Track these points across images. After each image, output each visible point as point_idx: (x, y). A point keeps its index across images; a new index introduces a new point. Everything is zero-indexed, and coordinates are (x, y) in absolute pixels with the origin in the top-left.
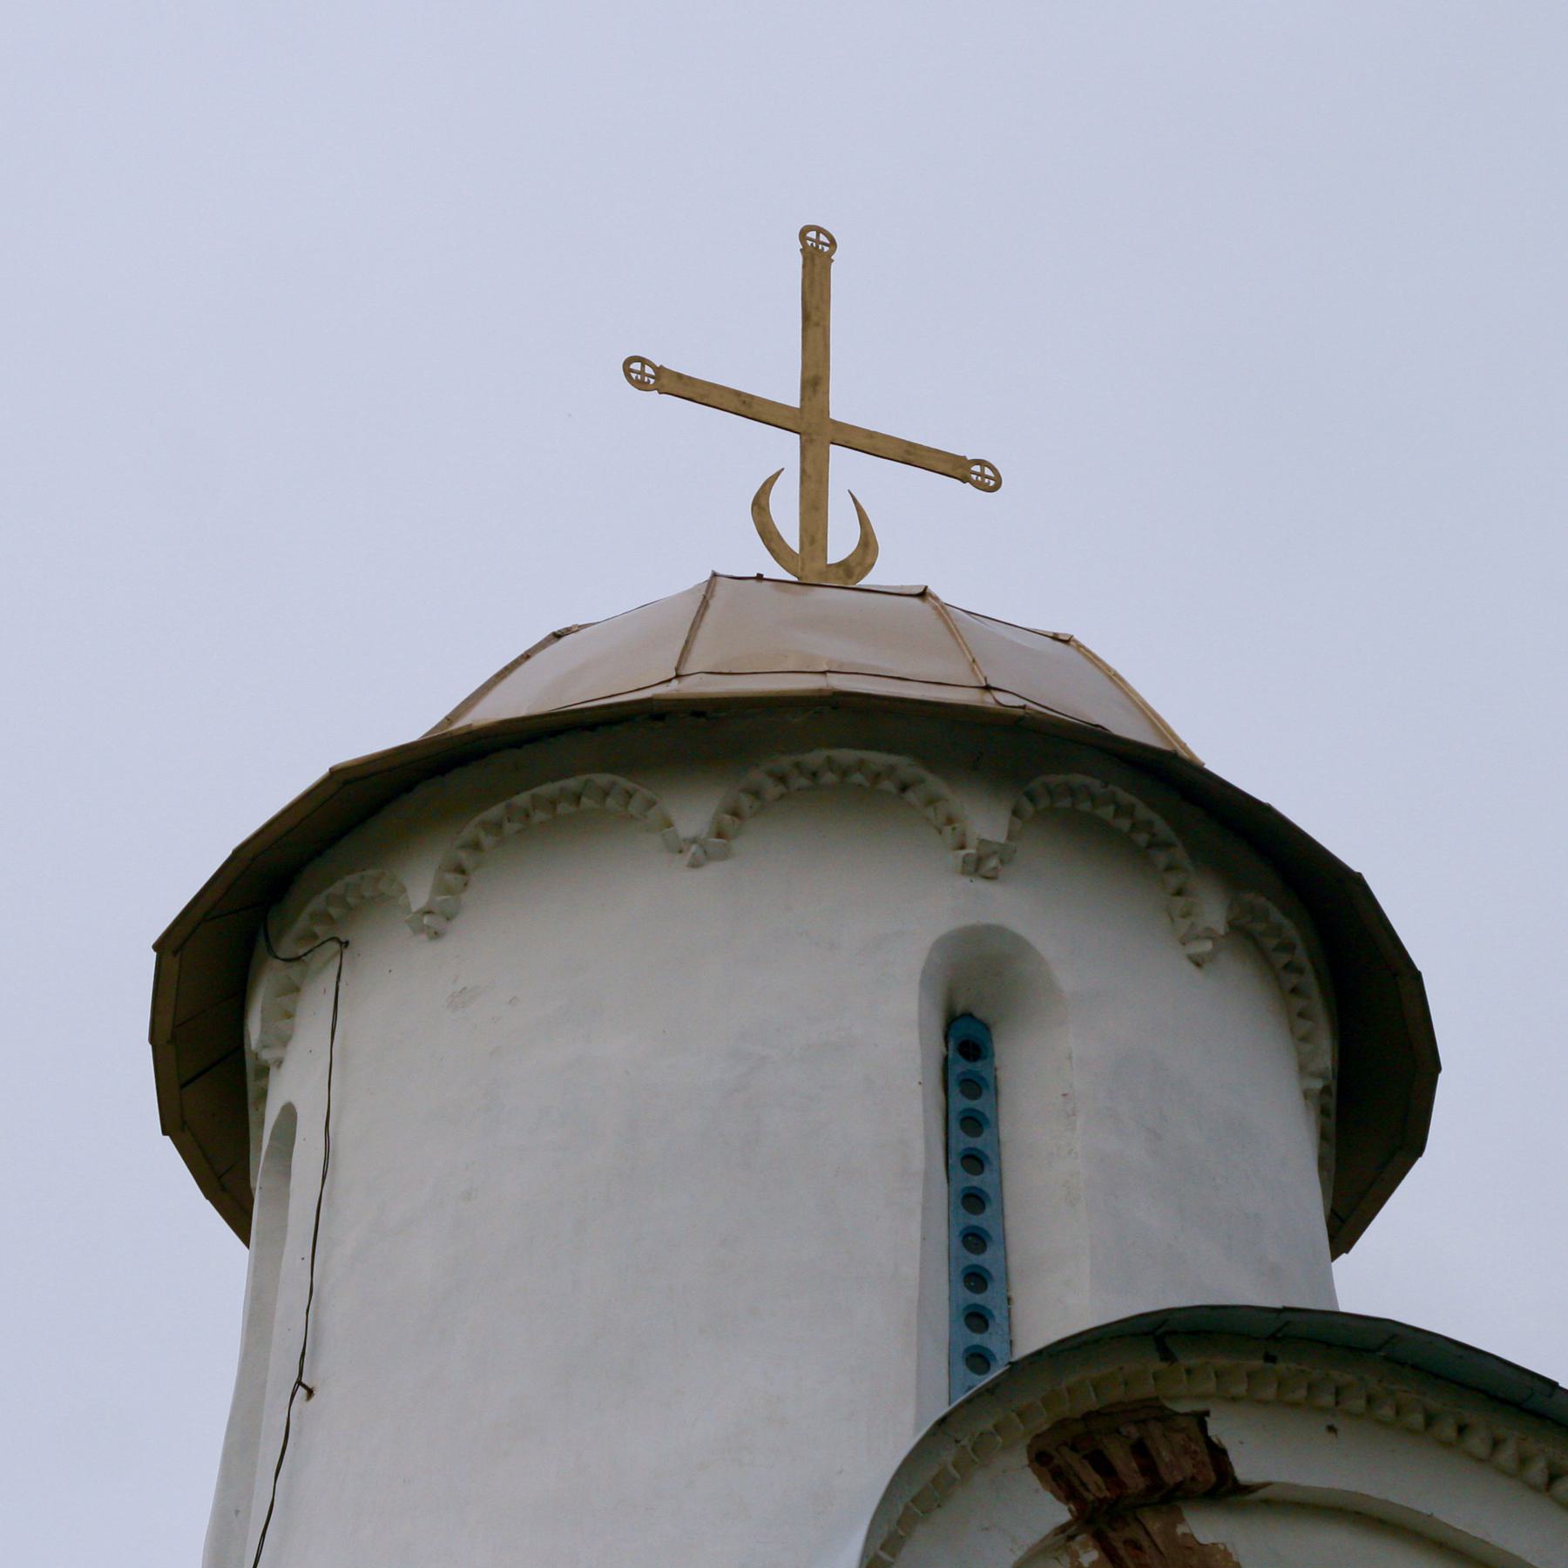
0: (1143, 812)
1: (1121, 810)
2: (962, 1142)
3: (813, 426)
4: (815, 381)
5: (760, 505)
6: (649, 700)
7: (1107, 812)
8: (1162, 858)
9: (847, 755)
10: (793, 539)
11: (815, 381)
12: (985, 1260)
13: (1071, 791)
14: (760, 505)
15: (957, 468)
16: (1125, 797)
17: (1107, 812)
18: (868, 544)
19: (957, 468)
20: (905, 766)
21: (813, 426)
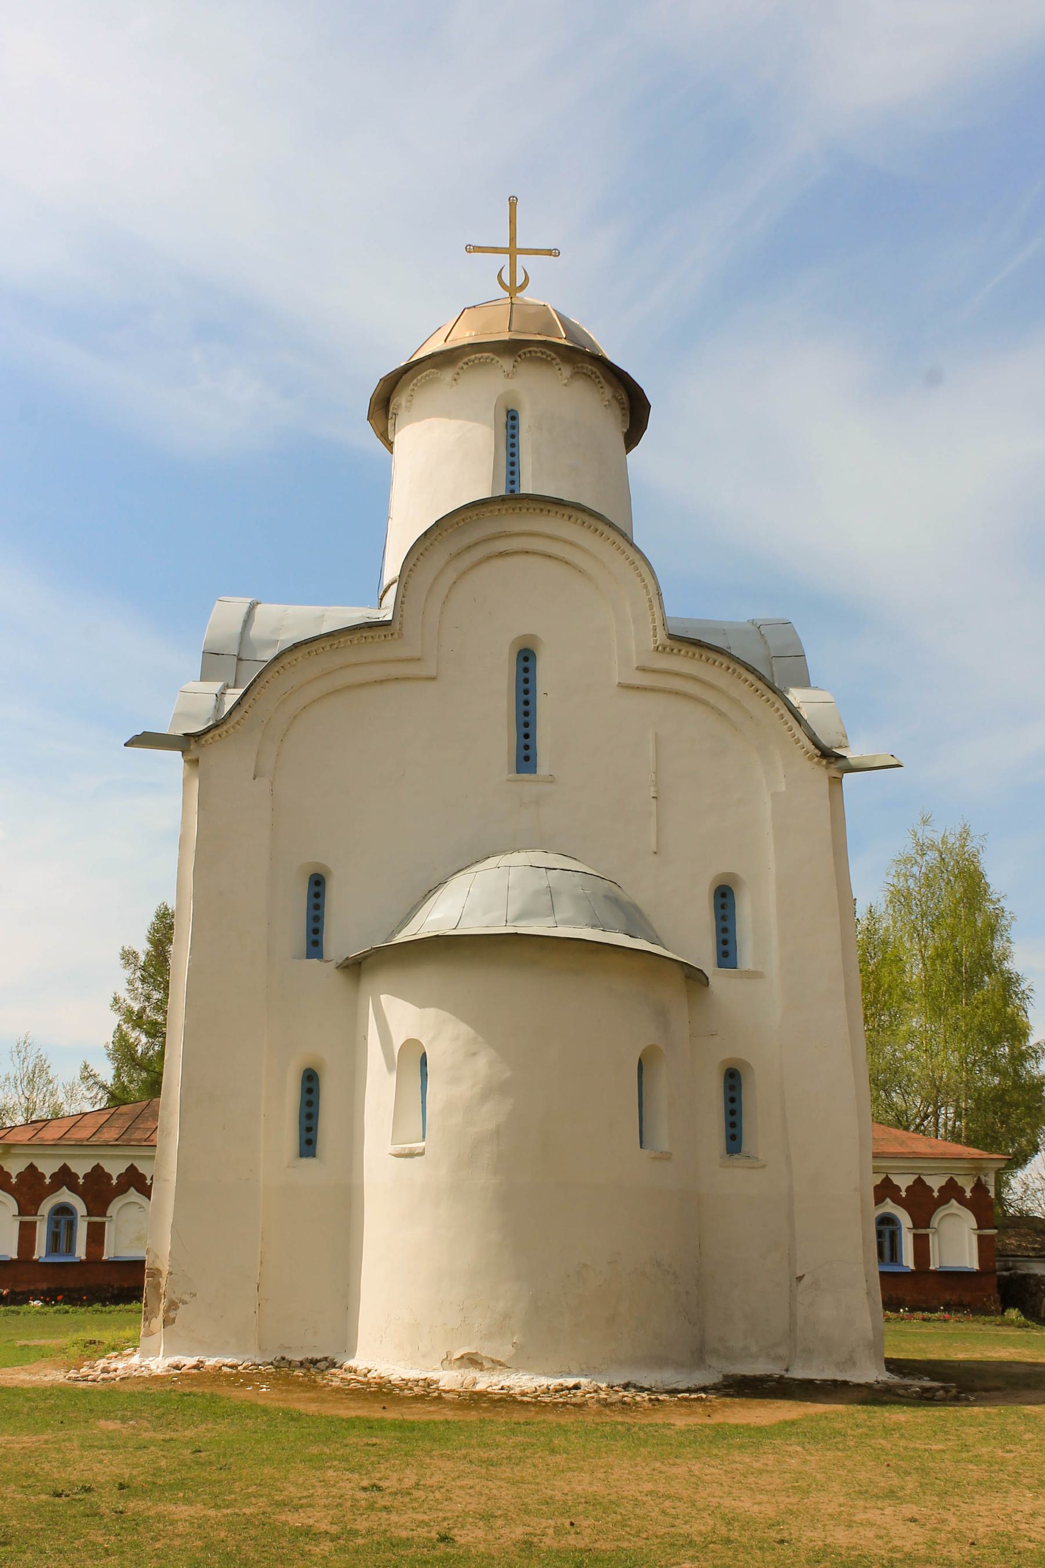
0: (549, 352)
1: (543, 353)
2: (511, 431)
3: (513, 251)
4: (513, 239)
5: (499, 275)
6: (1002, 1363)
7: (539, 355)
8: (554, 362)
9: (478, 355)
10: (508, 283)
11: (513, 239)
12: (727, 924)
13: (530, 352)
14: (499, 275)
15: (549, 252)
16: (544, 350)
17: (539, 355)
18: (527, 278)
19: (549, 252)
20: (491, 355)
21: (513, 251)
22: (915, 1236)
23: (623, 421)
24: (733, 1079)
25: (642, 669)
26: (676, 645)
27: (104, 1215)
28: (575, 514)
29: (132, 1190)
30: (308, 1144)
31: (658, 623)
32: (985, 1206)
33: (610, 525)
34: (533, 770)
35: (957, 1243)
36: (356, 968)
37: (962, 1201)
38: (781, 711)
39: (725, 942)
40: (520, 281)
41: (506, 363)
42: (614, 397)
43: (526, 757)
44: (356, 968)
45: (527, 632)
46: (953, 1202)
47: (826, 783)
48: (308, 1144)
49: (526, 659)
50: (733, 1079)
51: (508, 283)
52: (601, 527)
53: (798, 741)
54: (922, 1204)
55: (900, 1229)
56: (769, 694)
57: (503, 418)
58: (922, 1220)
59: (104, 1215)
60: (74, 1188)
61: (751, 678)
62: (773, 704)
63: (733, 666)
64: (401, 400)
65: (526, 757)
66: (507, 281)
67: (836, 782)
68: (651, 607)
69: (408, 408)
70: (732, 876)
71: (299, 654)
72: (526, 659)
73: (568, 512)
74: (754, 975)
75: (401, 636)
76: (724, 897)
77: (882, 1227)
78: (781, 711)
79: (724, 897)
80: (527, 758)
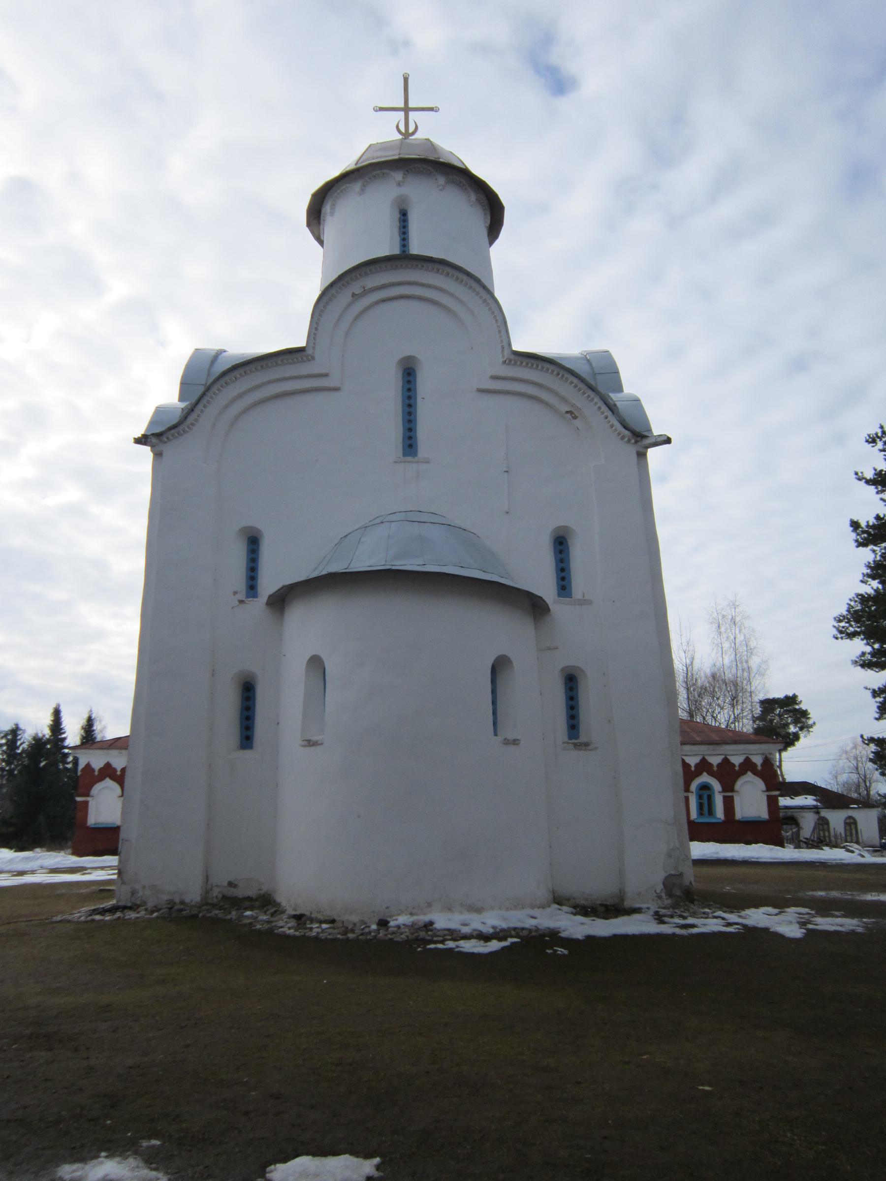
3: (406, 109)
4: (406, 101)
5: (397, 127)
10: (403, 131)
11: (406, 101)
14: (397, 127)
21: (406, 109)
22: (724, 797)
23: (485, 214)
24: (571, 681)
25: (495, 378)
26: (519, 359)
27: (88, 795)
28: (441, 267)
29: (705, 773)
30: (247, 739)
31: (505, 344)
32: (769, 773)
33: (468, 274)
34: (569, 595)
35: (751, 800)
36: (281, 601)
37: (756, 773)
38: (599, 405)
39: (410, 430)
40: (411, 129)
41: (398, 176)
42: (477, 200)
43: (410, 445)
44: (281, 601)
45: (409, 354)
46: (749, 773)
47: (634, 456)
48: (247, 739)
49: (409, 373)
50: (571, 681)
51: (403, 131)
52: (461, 275)
53: (612, 426)
54: (728, 775)
55: (713, 793)
56: (590, 392)
57: (397, 215)
58: (728, 786)
59: (88, 795)
60: (711, 773)
61: (575, 381)
62: (592, 400)
63: (562, 372)
64: (327, 208)
65: (410, 445)
66: (403, 130)
67: (642, 455)
68: (500, 332)
69: (332, 214)
70: (565, 528)
71: (236, 373)
72: (409, 374)
73: (436, 266)
74: (585, 602)
75: (313, 358)
76: (561, 544)
77: (702, 792)
78: (596, 400)
79: (561, 544)
80: (410, 446)
